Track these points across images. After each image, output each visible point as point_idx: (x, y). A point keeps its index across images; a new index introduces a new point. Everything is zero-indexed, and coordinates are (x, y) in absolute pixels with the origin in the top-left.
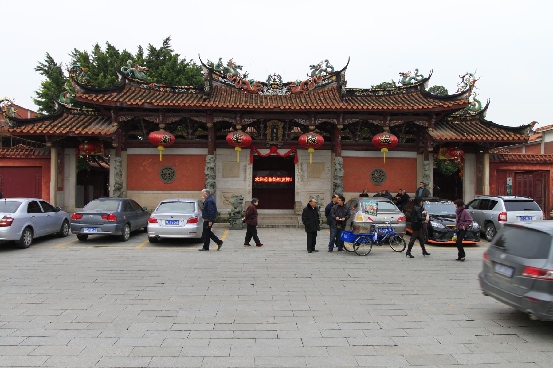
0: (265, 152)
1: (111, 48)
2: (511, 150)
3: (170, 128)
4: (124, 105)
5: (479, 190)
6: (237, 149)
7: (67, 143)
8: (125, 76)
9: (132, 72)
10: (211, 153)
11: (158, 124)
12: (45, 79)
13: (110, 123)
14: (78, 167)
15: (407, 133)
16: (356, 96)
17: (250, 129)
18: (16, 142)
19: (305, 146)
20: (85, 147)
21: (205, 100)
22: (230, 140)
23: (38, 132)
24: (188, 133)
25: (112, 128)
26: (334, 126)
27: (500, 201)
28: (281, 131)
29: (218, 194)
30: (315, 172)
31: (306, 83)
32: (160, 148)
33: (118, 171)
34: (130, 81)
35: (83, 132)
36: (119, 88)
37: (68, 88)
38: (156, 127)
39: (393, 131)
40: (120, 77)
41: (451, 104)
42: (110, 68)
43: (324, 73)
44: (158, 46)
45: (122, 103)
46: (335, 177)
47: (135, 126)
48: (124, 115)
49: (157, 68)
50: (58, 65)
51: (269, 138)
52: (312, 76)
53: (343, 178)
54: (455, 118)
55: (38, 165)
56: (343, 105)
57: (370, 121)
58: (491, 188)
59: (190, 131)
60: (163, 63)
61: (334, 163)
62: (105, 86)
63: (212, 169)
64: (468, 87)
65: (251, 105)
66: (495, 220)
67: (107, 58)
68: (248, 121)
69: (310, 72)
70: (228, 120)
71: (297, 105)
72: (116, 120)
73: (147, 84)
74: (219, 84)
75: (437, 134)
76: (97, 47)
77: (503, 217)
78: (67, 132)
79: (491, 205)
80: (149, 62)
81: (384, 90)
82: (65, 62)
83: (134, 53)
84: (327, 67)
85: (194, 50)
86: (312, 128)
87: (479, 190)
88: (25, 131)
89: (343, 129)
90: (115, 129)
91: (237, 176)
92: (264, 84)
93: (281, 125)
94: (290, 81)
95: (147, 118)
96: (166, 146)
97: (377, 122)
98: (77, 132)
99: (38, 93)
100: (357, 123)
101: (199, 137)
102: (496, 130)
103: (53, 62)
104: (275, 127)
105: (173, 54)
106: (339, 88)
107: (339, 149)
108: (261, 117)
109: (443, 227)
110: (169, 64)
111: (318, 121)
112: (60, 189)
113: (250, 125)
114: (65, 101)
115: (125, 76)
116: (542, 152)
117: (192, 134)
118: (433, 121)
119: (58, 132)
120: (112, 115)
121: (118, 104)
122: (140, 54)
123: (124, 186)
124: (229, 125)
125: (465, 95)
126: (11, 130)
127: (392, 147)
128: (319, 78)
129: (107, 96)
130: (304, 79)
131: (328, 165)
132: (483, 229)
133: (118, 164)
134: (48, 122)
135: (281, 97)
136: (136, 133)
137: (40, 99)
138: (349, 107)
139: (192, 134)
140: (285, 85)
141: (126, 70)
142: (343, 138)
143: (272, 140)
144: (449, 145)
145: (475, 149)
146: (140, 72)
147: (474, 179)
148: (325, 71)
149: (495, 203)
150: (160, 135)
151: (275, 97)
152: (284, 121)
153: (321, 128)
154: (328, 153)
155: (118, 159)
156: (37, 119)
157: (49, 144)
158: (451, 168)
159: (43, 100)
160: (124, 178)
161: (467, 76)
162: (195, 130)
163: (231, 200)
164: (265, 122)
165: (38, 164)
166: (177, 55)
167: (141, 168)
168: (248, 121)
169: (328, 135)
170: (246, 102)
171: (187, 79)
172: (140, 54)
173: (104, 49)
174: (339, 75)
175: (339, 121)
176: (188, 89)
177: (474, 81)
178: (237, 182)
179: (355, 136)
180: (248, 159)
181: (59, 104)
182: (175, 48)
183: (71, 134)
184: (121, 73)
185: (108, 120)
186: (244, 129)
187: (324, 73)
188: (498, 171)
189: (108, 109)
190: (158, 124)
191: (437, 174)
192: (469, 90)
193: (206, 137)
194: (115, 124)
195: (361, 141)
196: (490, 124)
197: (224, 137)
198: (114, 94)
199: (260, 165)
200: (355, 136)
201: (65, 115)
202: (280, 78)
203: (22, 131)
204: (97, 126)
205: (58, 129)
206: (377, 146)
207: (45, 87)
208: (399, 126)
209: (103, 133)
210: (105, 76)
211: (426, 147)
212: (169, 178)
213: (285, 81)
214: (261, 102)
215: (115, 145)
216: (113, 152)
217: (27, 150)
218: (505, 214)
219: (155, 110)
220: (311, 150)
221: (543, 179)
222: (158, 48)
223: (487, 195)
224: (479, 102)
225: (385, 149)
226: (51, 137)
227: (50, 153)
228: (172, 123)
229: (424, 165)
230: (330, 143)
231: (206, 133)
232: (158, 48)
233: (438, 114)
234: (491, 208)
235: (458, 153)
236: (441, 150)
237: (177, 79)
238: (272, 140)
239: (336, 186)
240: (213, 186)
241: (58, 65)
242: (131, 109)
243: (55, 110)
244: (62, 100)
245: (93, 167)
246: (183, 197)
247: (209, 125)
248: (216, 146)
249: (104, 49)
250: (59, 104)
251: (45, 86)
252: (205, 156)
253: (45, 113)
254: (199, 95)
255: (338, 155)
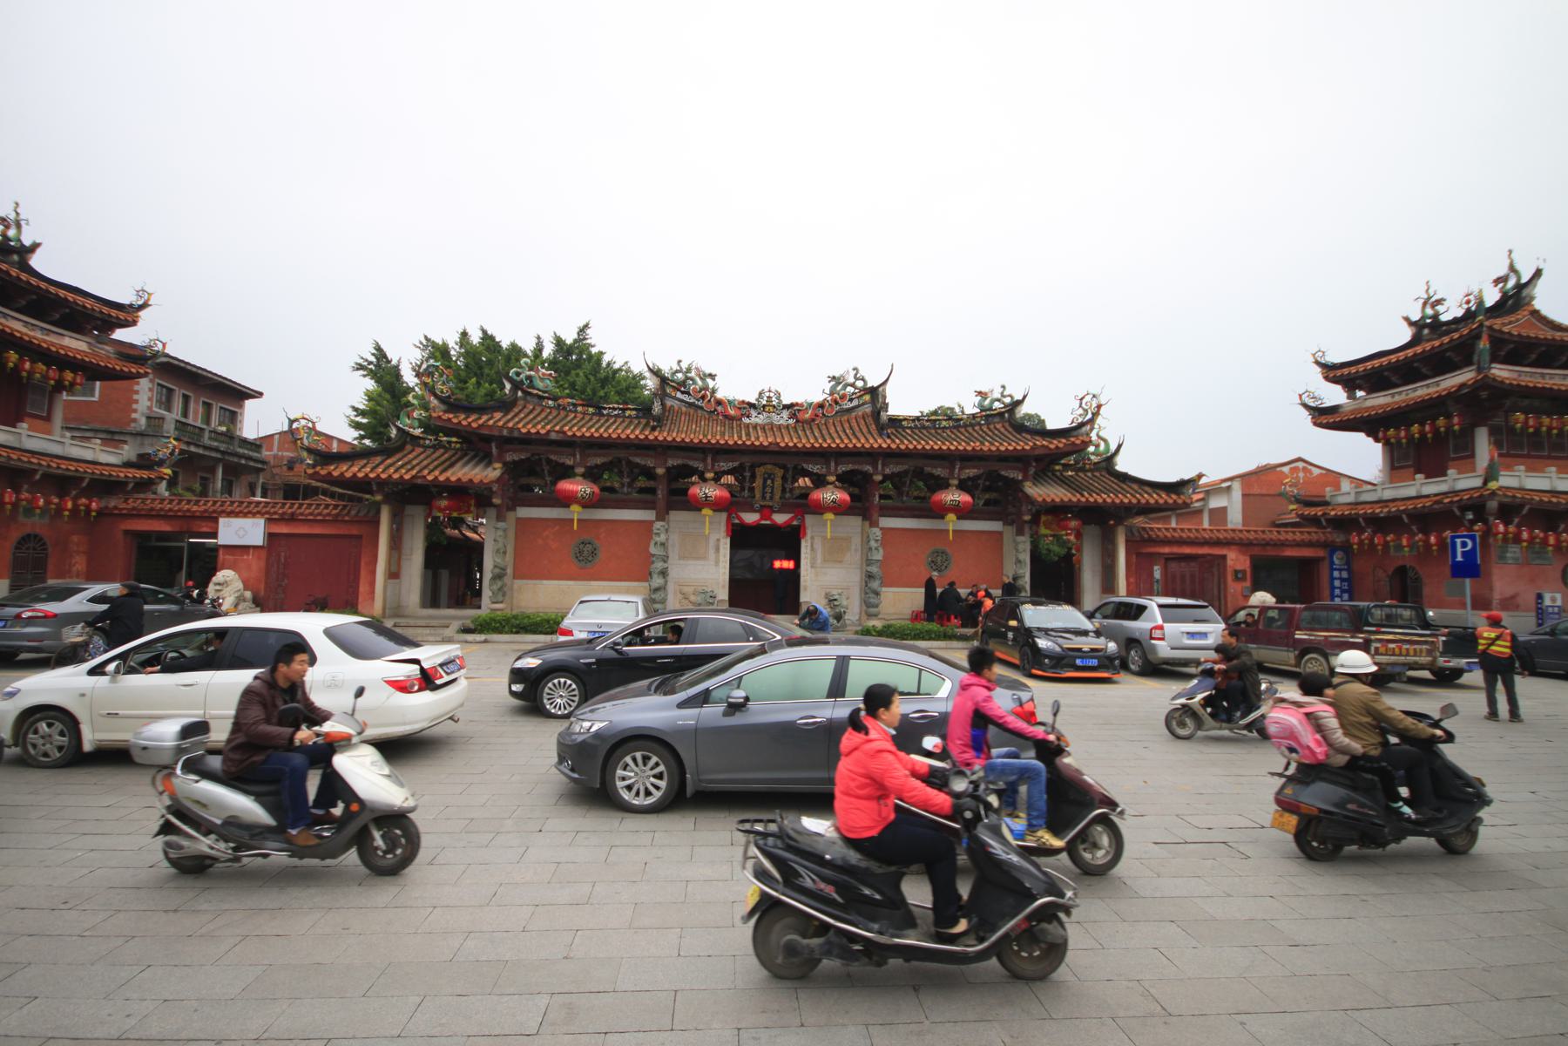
0: (750, 518)
1: (487, 338)
2: (1157, 520)
3: (592, 475)
4: (516, 434)
5: (1108, 586)
6: (707, 511)
7: (410, 495)
8: (517, 386)
9: (529, 378)
10: (660, 518)
11: (572, 468)
12: (370, 384)
13: (489, 464)
14: (428, 538)
15: (987, 489)
16: (904, 428)
17: (730, 479)
18: (310, 492)
19: (819, 509)
20: (444, 503)
21: (654, 429)
22: (695, 496)
23: (360, 475)
24: (623, 485)
25: (493, 473)
26: (867, 477)
27: (1153, 604)
28: (778, 482)
29: (671, 587)
30: (835, 552)
31: (821, 406)
32: (575, 508)
33: (500, 545)
34: (526, 393)
35: (442, 478)
36: (506, 406)
37: (415, 402)
38: (567, 473)
39: (963, 486)
40: (508, 386)
41: (1054, 444)
42: (486, 371)
43: (850, 389)
44: (569, 337)
45: (562, 432)
46: (869, 562)
47: (533, 469)
48: (514, 451)
49: (568, 373)
50: (394, 362)
51: (758, 495)
52: (831, 394)
53: (883, 563)
54: (1067, 467)
55: (355, 532)
56: (884, 443)
57: (928, 469)
58: (1128, 585)
59: (626, 480)
60: (578, 364)
61: (866, 540)
62: (478, 401)
63: (663, 544)
64: (1089, 416)
65: (732, 438)
66: (1144, 638)
67: (481, 354)
68: (725, 466)
69: (828, 387)
70: (691, 463)
71: (807, 441)
72: (500, 459)
73: (555, 399)
74: (676, 404)
75: (1042, 492)
76: (464, 334)
77: (1157, 634)
78: (413, 477)
79: (1137, 612)
80: (553, 364)
81: (950, 418)
82: (407, 358)
83: (528, 346)
84: (856, 379)
85: (630, 348)
86: (832, 478)
87: (1108, 586)
88: (335, 474)
89: (882, 482)
90: (497, 473)
91: (704, 558)
92: (752, 406)
93: (779, 473)
94: (794, 401)
95: (553, 457)
96: (585, 506)
97: (938, 472)
98: (430, 478)
99: (355, 409)
100: (906, 472)
101: (641, 491)
102: (1135, 487)
103: (385, 356)
104: (770, 476)
105: (594, 350)
106: (876, 414)
107: (875, 515)
108: (747, 460)
109: (1058, 649)
110: (587, 367)
111: (842, 469)
112: (394, 574)
113: (728, 472)
114: (410, 423)
115: (517, 386)
116: (1206, 525)
117: (630, 485)
118: (1032, 471)
119: (396, 476)
120: (494, 450)
121: (505, 432)
122: (539, 349)
123: (509, 571)
124: (692, 471)
125: (1084, 429)
126: (310, 471)
127: (963, 513)
128: (843, 397)
129: (485, 418)
130: (818, 397)
131: (856, 541)
132: (1123, 653)
133: (500, 533)
134: (379, 459)
135: (779, 427)
136: (532, 480)
137: (359, 419)
138: (893, 446)
139: (630, 485)
140: (786, 407)
141: (518, 374)
142: (881, 497)
143: (764, 498)
144: (1058, 511)
145: (1101, 518)
146: (544, 379)
147: (1099, 568)
148: (853, 385)
149: (1141, 609)
150: (578, 487)
151: (771, 428)
152: (784, 467)
153: (845, 480)
154: (854, 523)
155: (501, 525)
156: (351, 455)
157: (379, 498)
158: (1056, 548)
159: (365, 421)
160: (510, 557)
161: (1088, 398)
162: (634, 480)
163: (693, 598)
164: (753, 467)
165: (354, 531)
166: (601, 353)
167: (540, 542)
168: (725, 466)
169: (856, 491)
170: (723, 434)
171: (618, 393)
172: (539, 349)
173: (475, 338)
174: (875, 393)
175: (875, 468)
176: (624, 410)
177: (1099, 407)
178: (702, 564)
179: (900, 494)
180: (723, 528)
181: (399, 429)
182: (599, 342)
183: (419, 481)
184: (510, 380)
185: (486, 458)
186: (717, 479)
187: (850, 389)
188: (1139, 554)
189: (487, 439)
190: (572, 468)
191: (1038, 560)
192: (1092, 421)
193: (652, 491)
194: (498, 465)
195: (914, 503)
196: (1125, 478)
197: (685, 492)
198: (498, 415)
199: (740, 537)
200: (900, 494)
201: (409, 447)
202: (778, 395)
203: (330, 474)
204: (466, 469)
205: (397, 469)
206: (939, 512)
207: (370, 399)
208: (974, 479)
209: (476, 481)
210: (478, 384)
211: (1020, 514)
212: (588, 560)
213: (786, 401)
214: (748, 435)
215: (497, 501)
216: (492, 512)
217: (327, 506)
218: (1161, 628)
219: (569, 444)
220: (829, 516)
221: (1215, 570)
222: (569, 341)
223: (1122, 595)
224: (1105, 441)
225: (951, 517)
226: (382, 484)
227: (378, 512)
228: (597, 466)
229: (1017, 544)
230: (860, 505)
231: (651, 484)
232: (569, 341)
233: (1038, 459)
234: (1136, 617)
235: (1073, 524)
236: (1043, 518)
237: (602, 393)
238: (764, 498)
239: (870, 576)
240: (664, 573)
241: (394, 362)
242: (526, 440)
243: (389, 439)
244: (404, 422)
245: (450, 538)
246: (619, 592)
247: (660, 471)
248: (671, 506)
249: (475, 338)
250: (399, 429)
251: (370, 397)
252: (651, 523)
253: (367, 442)
254: (644, 421)
255: (874, 524)
